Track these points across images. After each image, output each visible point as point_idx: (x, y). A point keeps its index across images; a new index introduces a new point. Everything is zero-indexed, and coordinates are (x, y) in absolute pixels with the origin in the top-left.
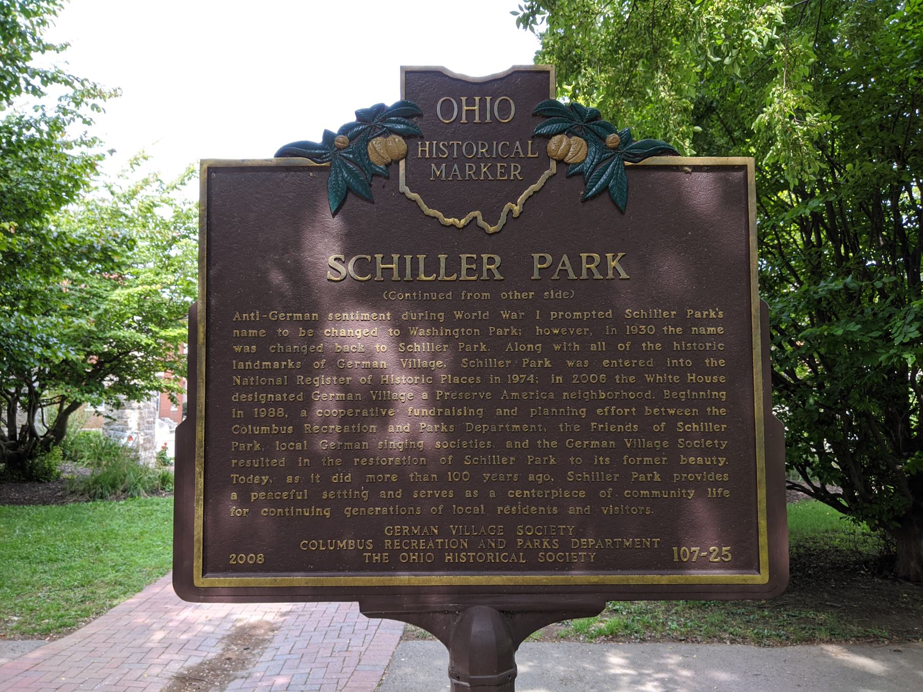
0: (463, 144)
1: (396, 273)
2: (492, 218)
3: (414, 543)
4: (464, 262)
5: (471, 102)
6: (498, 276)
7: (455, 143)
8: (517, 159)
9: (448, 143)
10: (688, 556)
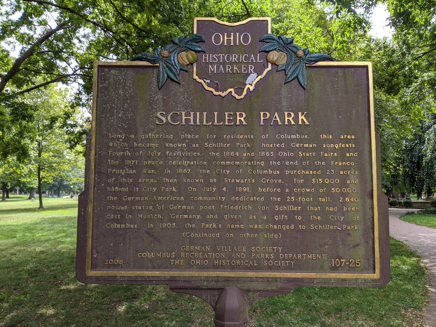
0: (225, 55)
1: (192, 121)
2: (239, 91)
3: (196, 254)
4: (226, 116)
5: (229, 36)
6: (244, 123)
7: (221, 55)
8: (252, 63)
9: (218, 55)
10: (339, 264)
